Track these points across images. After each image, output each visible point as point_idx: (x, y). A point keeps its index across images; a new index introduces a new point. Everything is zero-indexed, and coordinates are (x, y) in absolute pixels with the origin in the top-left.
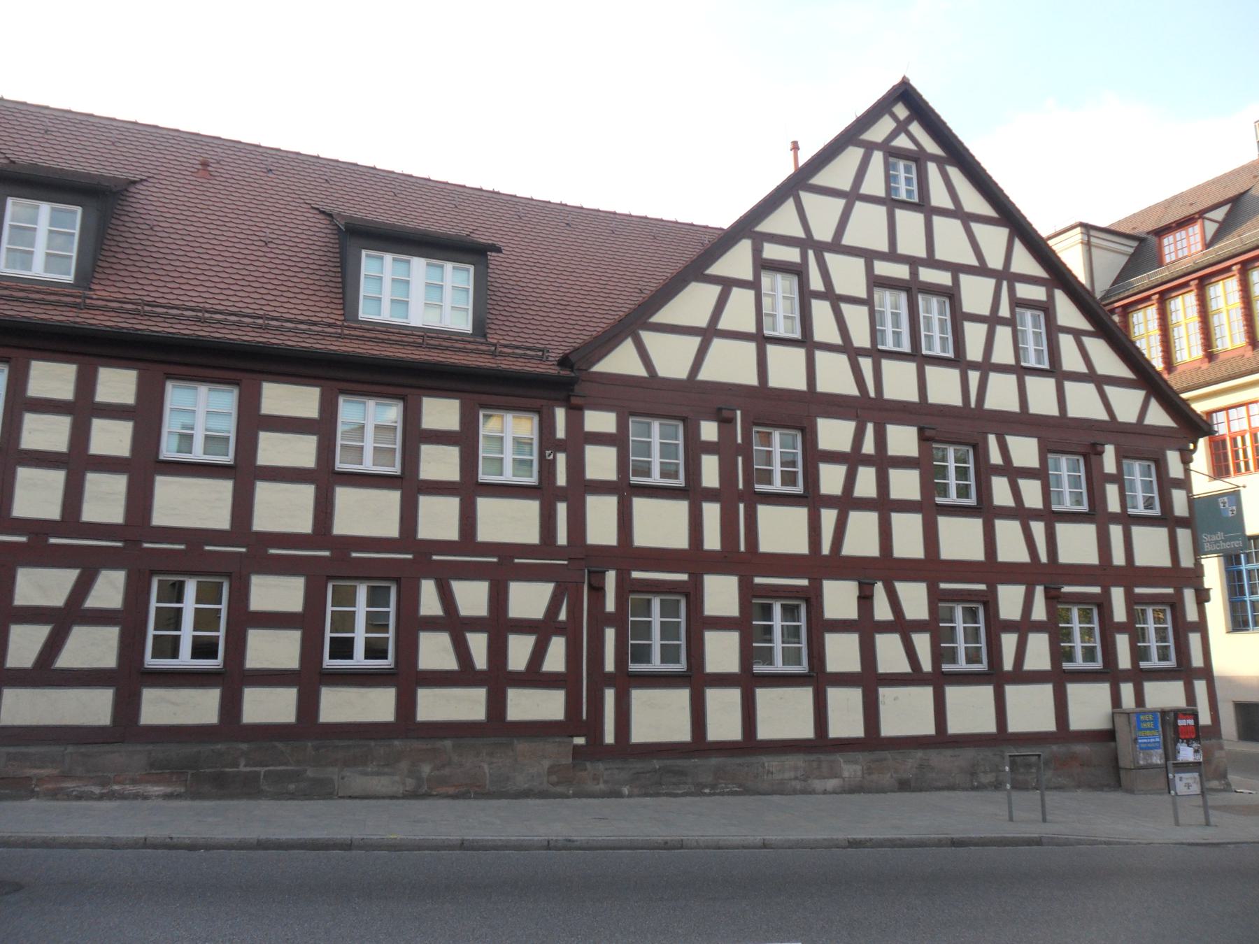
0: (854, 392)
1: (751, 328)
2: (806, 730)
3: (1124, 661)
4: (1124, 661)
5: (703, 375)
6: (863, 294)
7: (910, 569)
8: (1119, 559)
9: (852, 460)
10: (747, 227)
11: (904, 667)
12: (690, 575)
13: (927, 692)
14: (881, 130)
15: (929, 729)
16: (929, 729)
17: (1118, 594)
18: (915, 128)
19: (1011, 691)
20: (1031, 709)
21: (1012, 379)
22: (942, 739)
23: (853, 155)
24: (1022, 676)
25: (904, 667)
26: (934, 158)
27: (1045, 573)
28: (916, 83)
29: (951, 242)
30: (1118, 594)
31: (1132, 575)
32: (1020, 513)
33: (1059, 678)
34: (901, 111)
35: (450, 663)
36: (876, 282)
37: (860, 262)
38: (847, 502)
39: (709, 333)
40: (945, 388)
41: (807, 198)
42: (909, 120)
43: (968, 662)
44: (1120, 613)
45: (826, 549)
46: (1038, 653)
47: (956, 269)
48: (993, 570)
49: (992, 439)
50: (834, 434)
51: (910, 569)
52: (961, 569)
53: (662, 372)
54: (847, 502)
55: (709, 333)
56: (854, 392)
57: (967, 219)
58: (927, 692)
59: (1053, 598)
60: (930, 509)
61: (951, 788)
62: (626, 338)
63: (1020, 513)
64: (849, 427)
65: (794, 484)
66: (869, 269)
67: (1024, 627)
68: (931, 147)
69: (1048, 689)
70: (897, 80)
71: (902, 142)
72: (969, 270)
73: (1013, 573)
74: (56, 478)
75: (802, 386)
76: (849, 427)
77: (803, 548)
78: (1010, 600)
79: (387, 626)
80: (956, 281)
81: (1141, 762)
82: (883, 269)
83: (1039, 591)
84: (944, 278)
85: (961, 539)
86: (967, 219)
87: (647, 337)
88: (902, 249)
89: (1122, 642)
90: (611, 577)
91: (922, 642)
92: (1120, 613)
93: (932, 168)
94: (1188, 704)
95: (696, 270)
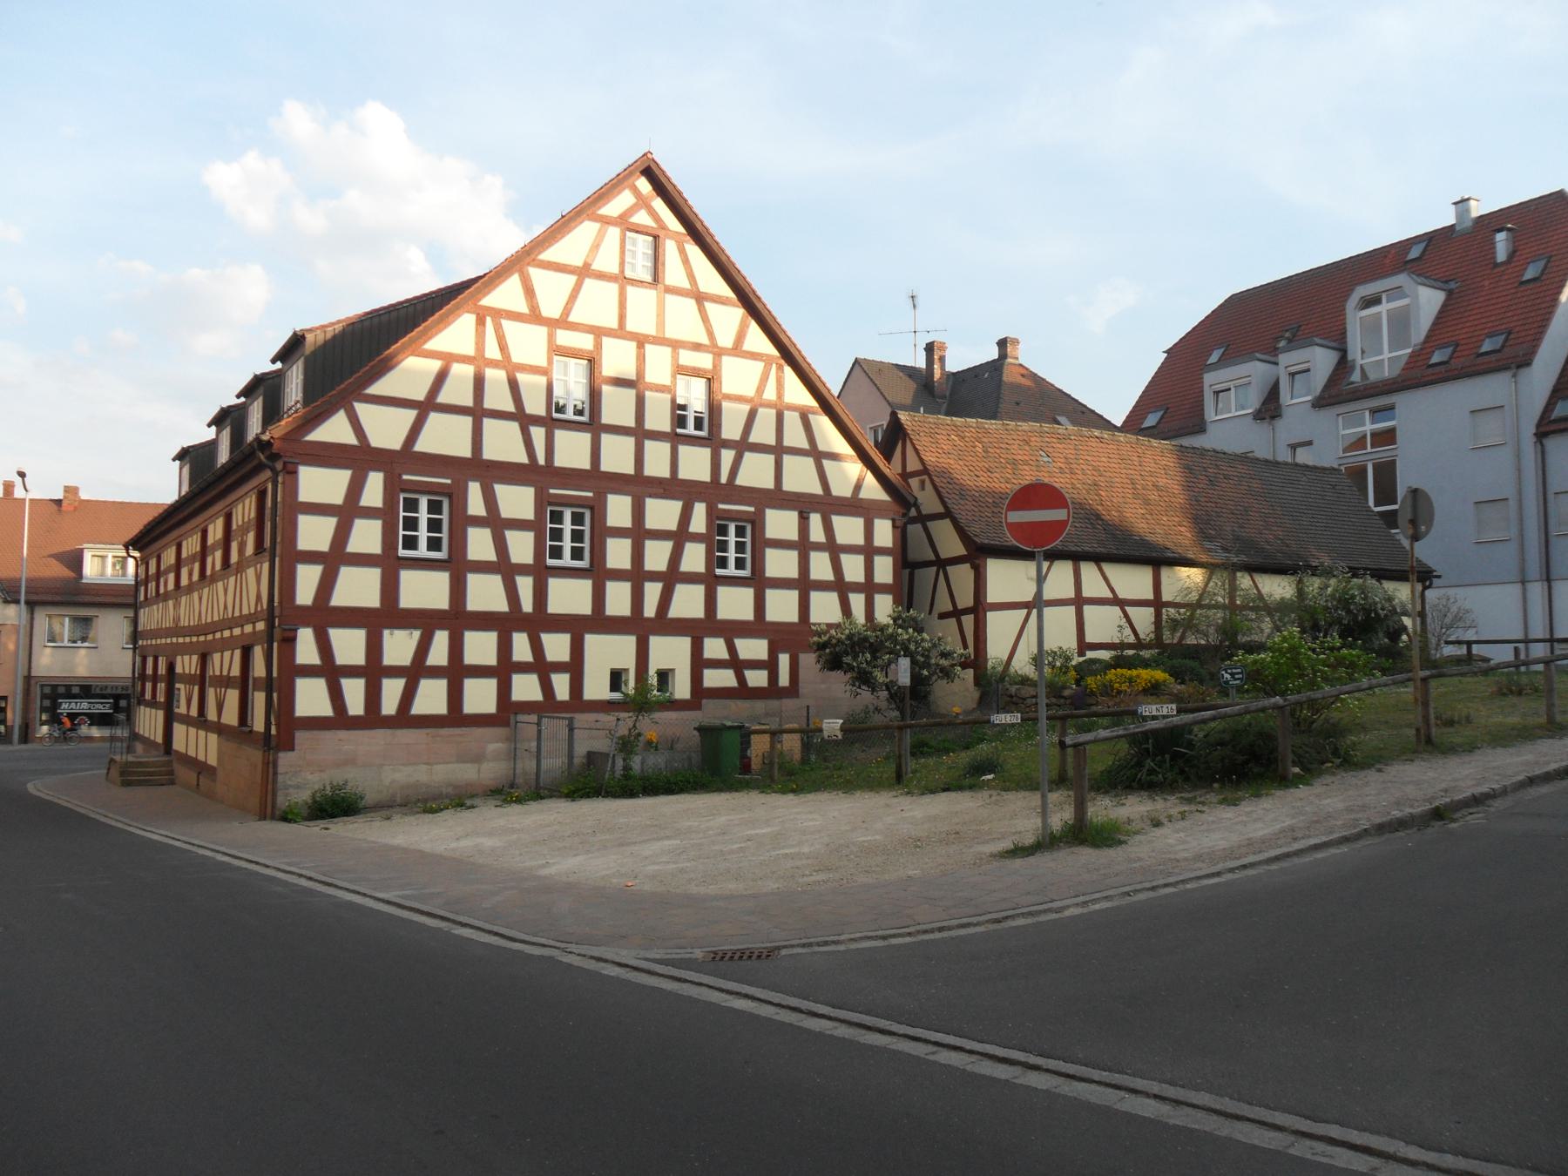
0: (524, 459)
1: (630, 422)
5: (421, 446)
6: (543, 362)
14: (621, 203)
18: (659, 205)
23: (586, 231)
26: (674, 235)
29: (683, 320)
34: (644, 185)
35: (325, 709)
36: (556, 350)
37: (633, 345)
39: (426, 406)
41: (535, 273)
47: (598, 332)
53: (376, 441)
55: (426, 406)
56: (524, 459)
57: (700, 298)
62: (337, 410)
64: (676, 506)
66: (675, 357)
68: (674, 224)
71: (642, 218)
72: (610, 333)
74: (793, 596)
75: (770, 485)
76: (676, 506)
80: (598, 345)
82: (565, 338)
84: (585, 342)
86: (700, 298)
87: (361, 408)
88: (631, 326)
93: (670, 247)
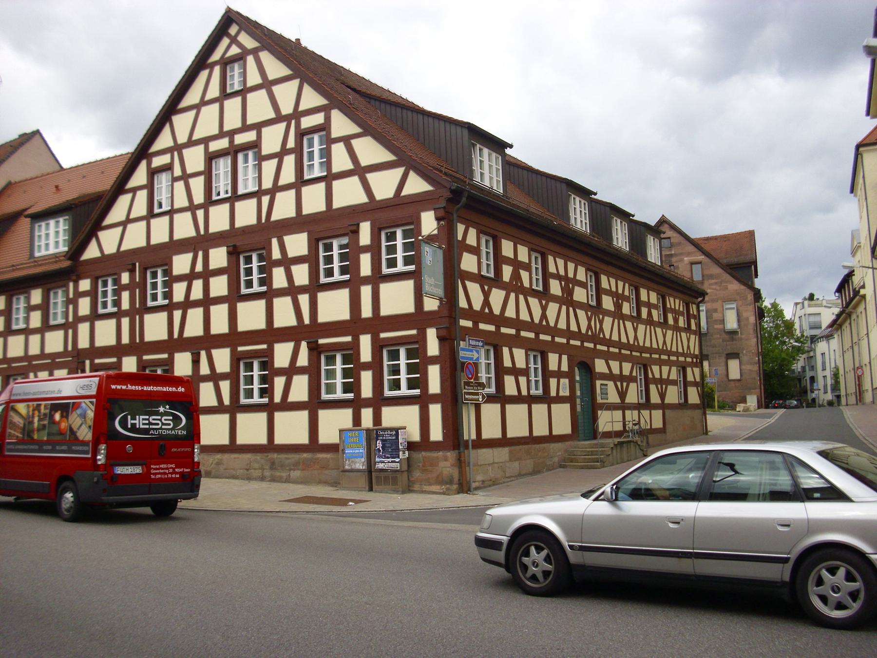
2: (304, 439)
3: (367, 391)
4: (367, 391)
7: (219, 341)
8: (366, 312)
9: (190, 277)
10: (143, 152)
11: (214, 402)
12: (353, 336)
13: (226, 417)
15: (226, 441)
16: (226, 441)
17: (365, 341)
19: (278, 416)
20: (292, 428)
21: (355, 180)
22: (270, 447)
24: (287, 406)
25: (214, 402)
27: (308, 332)
28: (235, 8)
30: (365, 341)
31: (378, 323)
32: (292, 291)
33: (315, 404)
38: (187, 304)
40: (314, 200)
42: (229, 36)
43: (409, 388)
44: (366, 354)
45: (176, 336)
46: (300, 389)
48: (272, 334)
49: (275, 241)
50: (181, 263)
51: (219, 341)
52: (252, 336)
54: (187, 304)
58: (226, 417)
59: (315, 350)
60: (234, 298)
61: (234, 477)
63: (292, 291)
65: (389, 267)
67: (291, 371)
69: (304, 415)
70: (222, 12)
73: (285, 334)
77: (165, 336)
78: (282, 354)
79: (399, 371)
81: (347, 467)
83: (304, 345)
85: (252, 316)
89: (367, 378)
90: (88, 362)
91: (225, 386)
92: (366, 354)
94: (375, 425)
95: (120, 187)
